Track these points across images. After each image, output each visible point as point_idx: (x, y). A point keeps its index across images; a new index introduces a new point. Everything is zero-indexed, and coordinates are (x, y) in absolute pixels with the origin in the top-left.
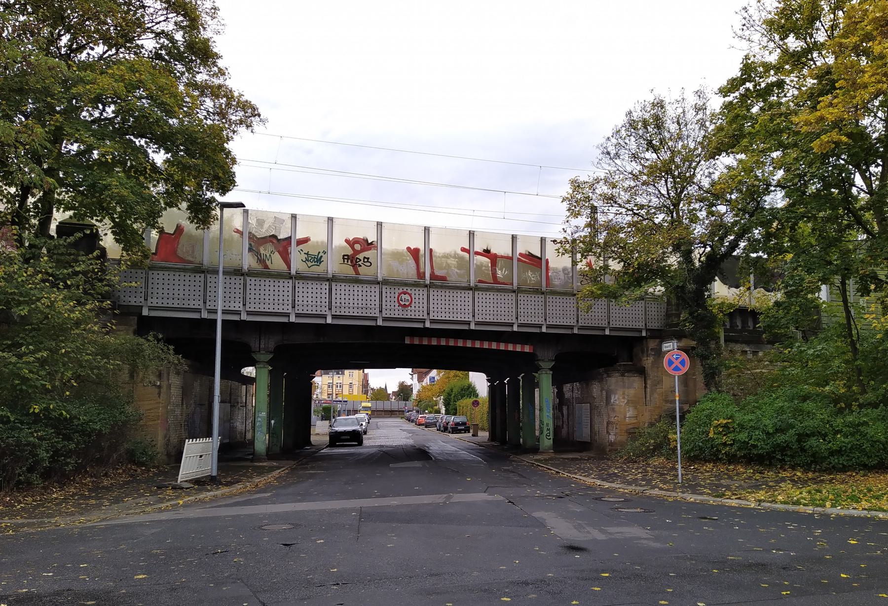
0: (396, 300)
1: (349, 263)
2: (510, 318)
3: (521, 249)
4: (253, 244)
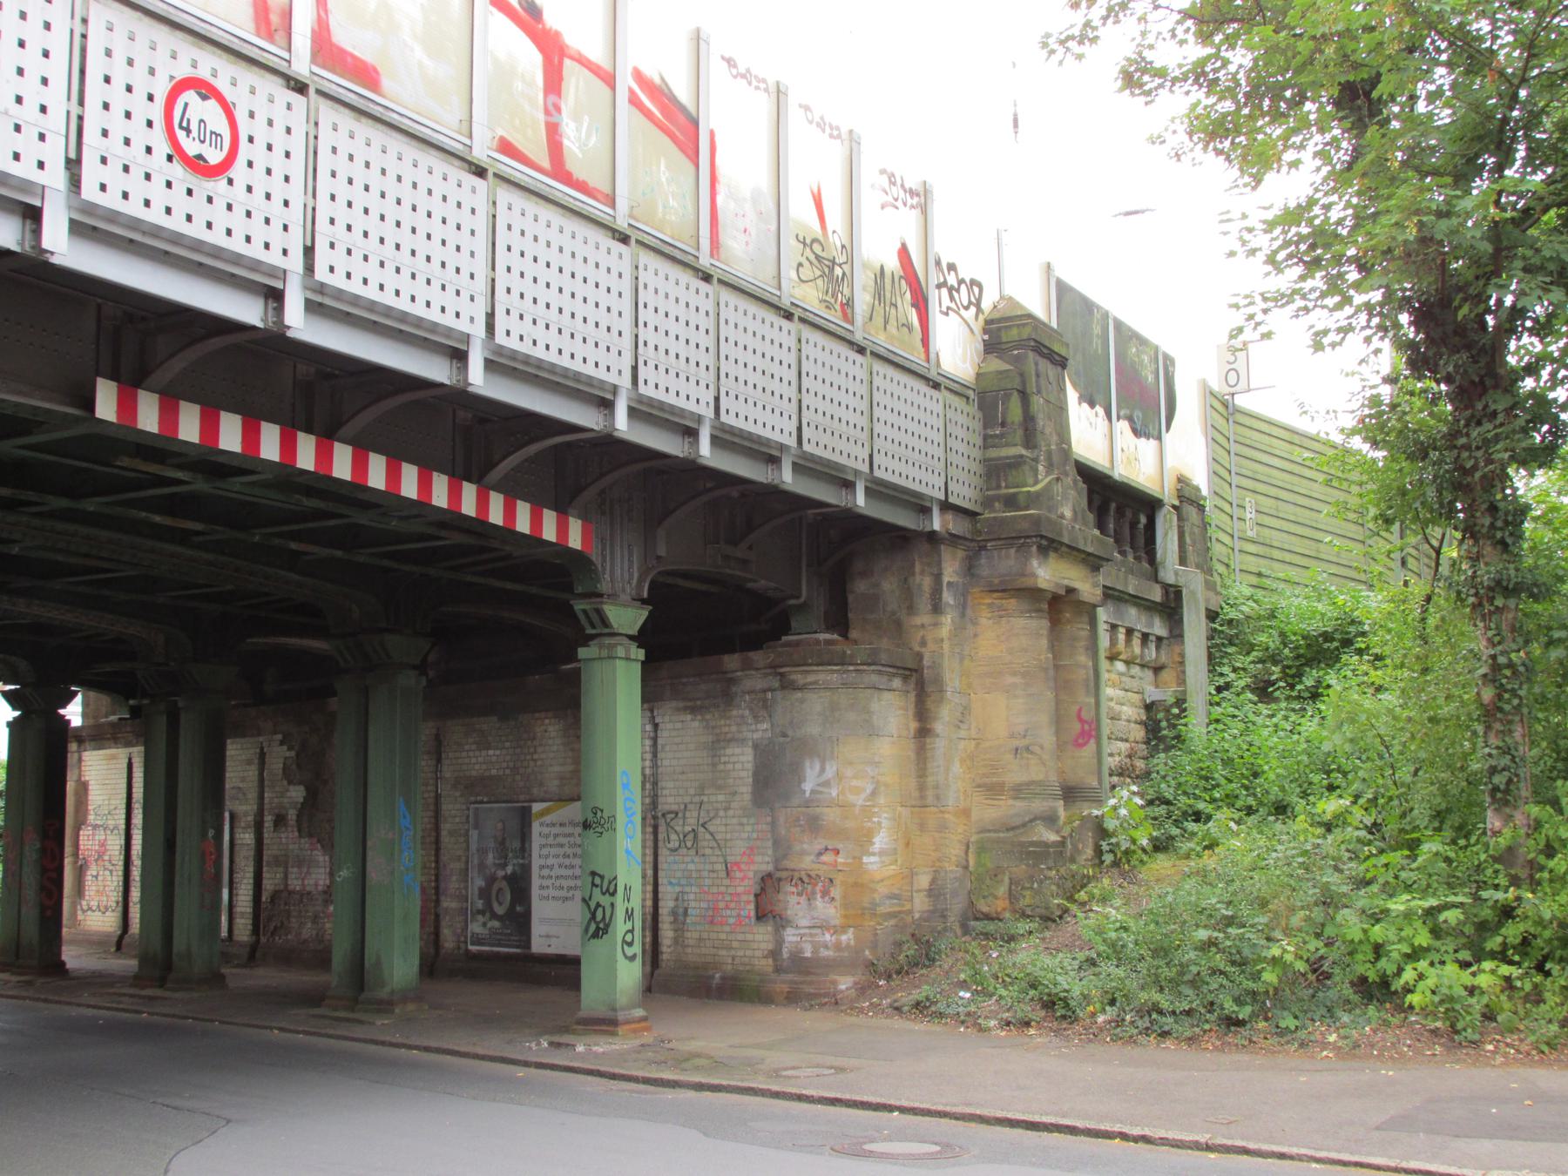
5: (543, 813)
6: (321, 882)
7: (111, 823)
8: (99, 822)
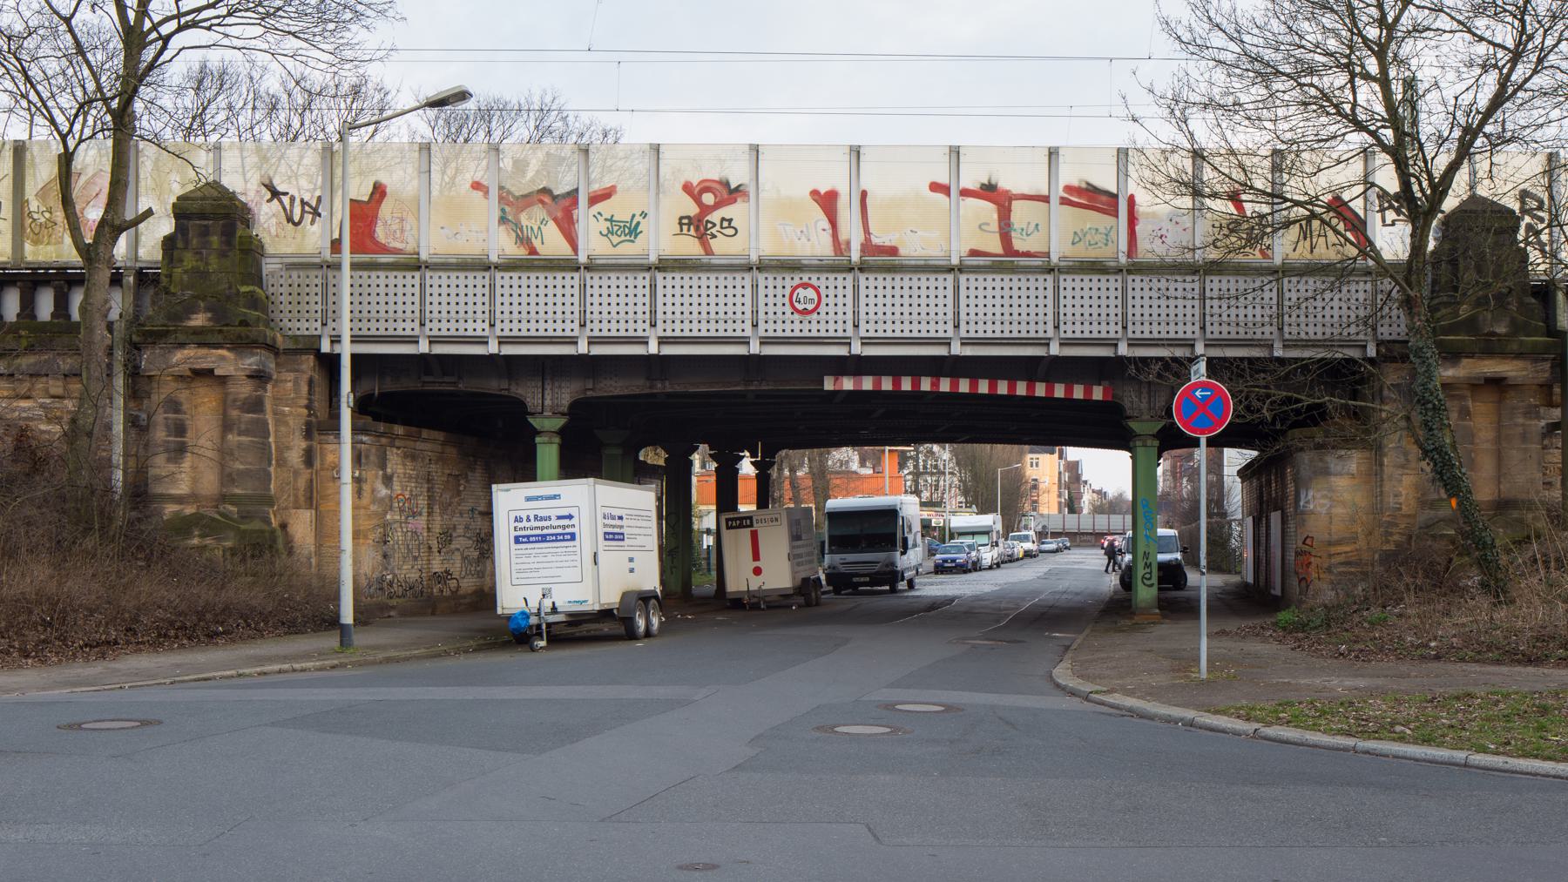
0: (786, 300)
1: (692, 232)
2: (1041, 327)
3: (1070, 174)
4: (508, 209)
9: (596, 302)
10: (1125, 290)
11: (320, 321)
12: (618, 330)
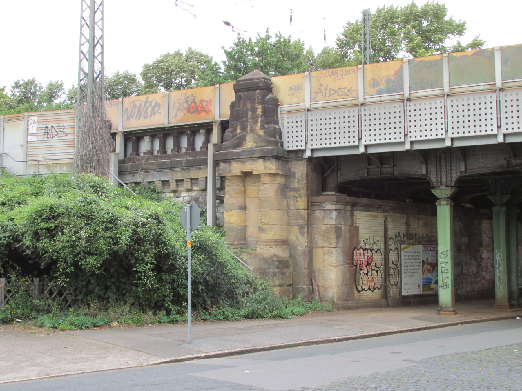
5: (405, 248)
6: (474, 271)
7: (375, 248)
8: (367, 247)
9: (368, 124)
10: (446, 107)
11: (444, 129)
12: (475, 132)
